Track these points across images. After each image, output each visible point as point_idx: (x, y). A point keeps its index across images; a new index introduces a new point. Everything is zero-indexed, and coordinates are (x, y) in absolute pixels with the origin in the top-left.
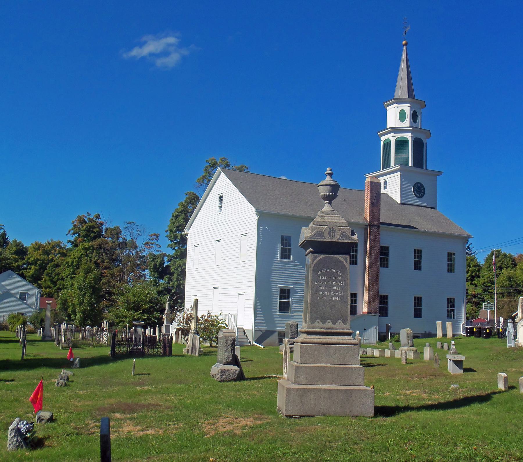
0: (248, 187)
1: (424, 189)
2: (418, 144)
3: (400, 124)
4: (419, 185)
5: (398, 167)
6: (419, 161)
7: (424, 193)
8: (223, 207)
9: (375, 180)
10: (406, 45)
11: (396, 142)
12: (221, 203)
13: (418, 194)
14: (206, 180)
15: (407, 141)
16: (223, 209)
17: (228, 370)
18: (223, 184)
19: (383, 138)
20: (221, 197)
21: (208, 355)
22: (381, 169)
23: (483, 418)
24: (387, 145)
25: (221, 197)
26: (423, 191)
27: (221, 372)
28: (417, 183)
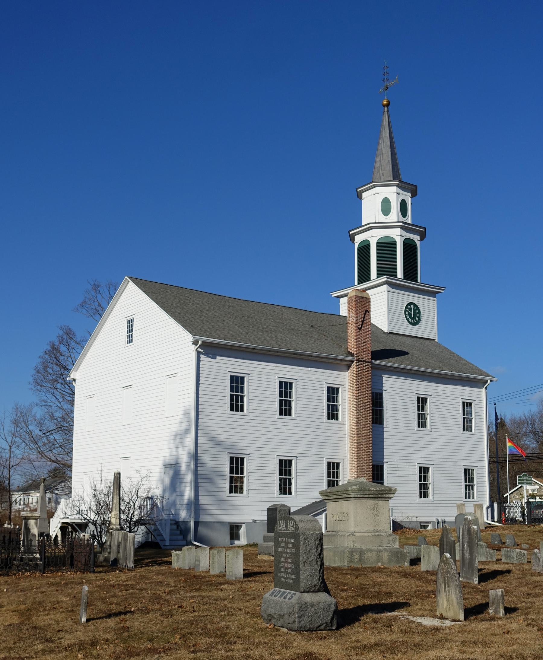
0: (174, 304)
1: (419, 312)
2: (410, 248)
3: (382, 218)
4: (412, 306)
5: (384, 279)
6: (411, 272)
7: (419, 318)
8: (134, 336)
9: (364, 295)
10: (388, 105)
11: (379, 244)
12: (132, 331)
13: (412, 319)
14: (96, 307)
15: (394, 244)
16: (134, 338)
17: (313, 605)
18: (132, 300)
19: (359, 239)
20: (130, 323)
21: (381, 572)
22: (356, 283)
23: (470, 650)
24: (365, 249)
25: (130, 323)
26: (418, 315)
27: (300, 609)
28: (410, 304)
